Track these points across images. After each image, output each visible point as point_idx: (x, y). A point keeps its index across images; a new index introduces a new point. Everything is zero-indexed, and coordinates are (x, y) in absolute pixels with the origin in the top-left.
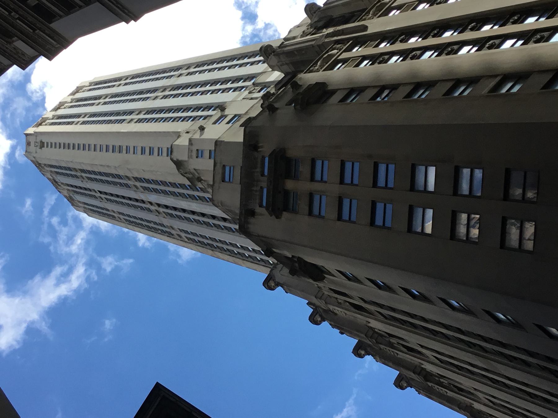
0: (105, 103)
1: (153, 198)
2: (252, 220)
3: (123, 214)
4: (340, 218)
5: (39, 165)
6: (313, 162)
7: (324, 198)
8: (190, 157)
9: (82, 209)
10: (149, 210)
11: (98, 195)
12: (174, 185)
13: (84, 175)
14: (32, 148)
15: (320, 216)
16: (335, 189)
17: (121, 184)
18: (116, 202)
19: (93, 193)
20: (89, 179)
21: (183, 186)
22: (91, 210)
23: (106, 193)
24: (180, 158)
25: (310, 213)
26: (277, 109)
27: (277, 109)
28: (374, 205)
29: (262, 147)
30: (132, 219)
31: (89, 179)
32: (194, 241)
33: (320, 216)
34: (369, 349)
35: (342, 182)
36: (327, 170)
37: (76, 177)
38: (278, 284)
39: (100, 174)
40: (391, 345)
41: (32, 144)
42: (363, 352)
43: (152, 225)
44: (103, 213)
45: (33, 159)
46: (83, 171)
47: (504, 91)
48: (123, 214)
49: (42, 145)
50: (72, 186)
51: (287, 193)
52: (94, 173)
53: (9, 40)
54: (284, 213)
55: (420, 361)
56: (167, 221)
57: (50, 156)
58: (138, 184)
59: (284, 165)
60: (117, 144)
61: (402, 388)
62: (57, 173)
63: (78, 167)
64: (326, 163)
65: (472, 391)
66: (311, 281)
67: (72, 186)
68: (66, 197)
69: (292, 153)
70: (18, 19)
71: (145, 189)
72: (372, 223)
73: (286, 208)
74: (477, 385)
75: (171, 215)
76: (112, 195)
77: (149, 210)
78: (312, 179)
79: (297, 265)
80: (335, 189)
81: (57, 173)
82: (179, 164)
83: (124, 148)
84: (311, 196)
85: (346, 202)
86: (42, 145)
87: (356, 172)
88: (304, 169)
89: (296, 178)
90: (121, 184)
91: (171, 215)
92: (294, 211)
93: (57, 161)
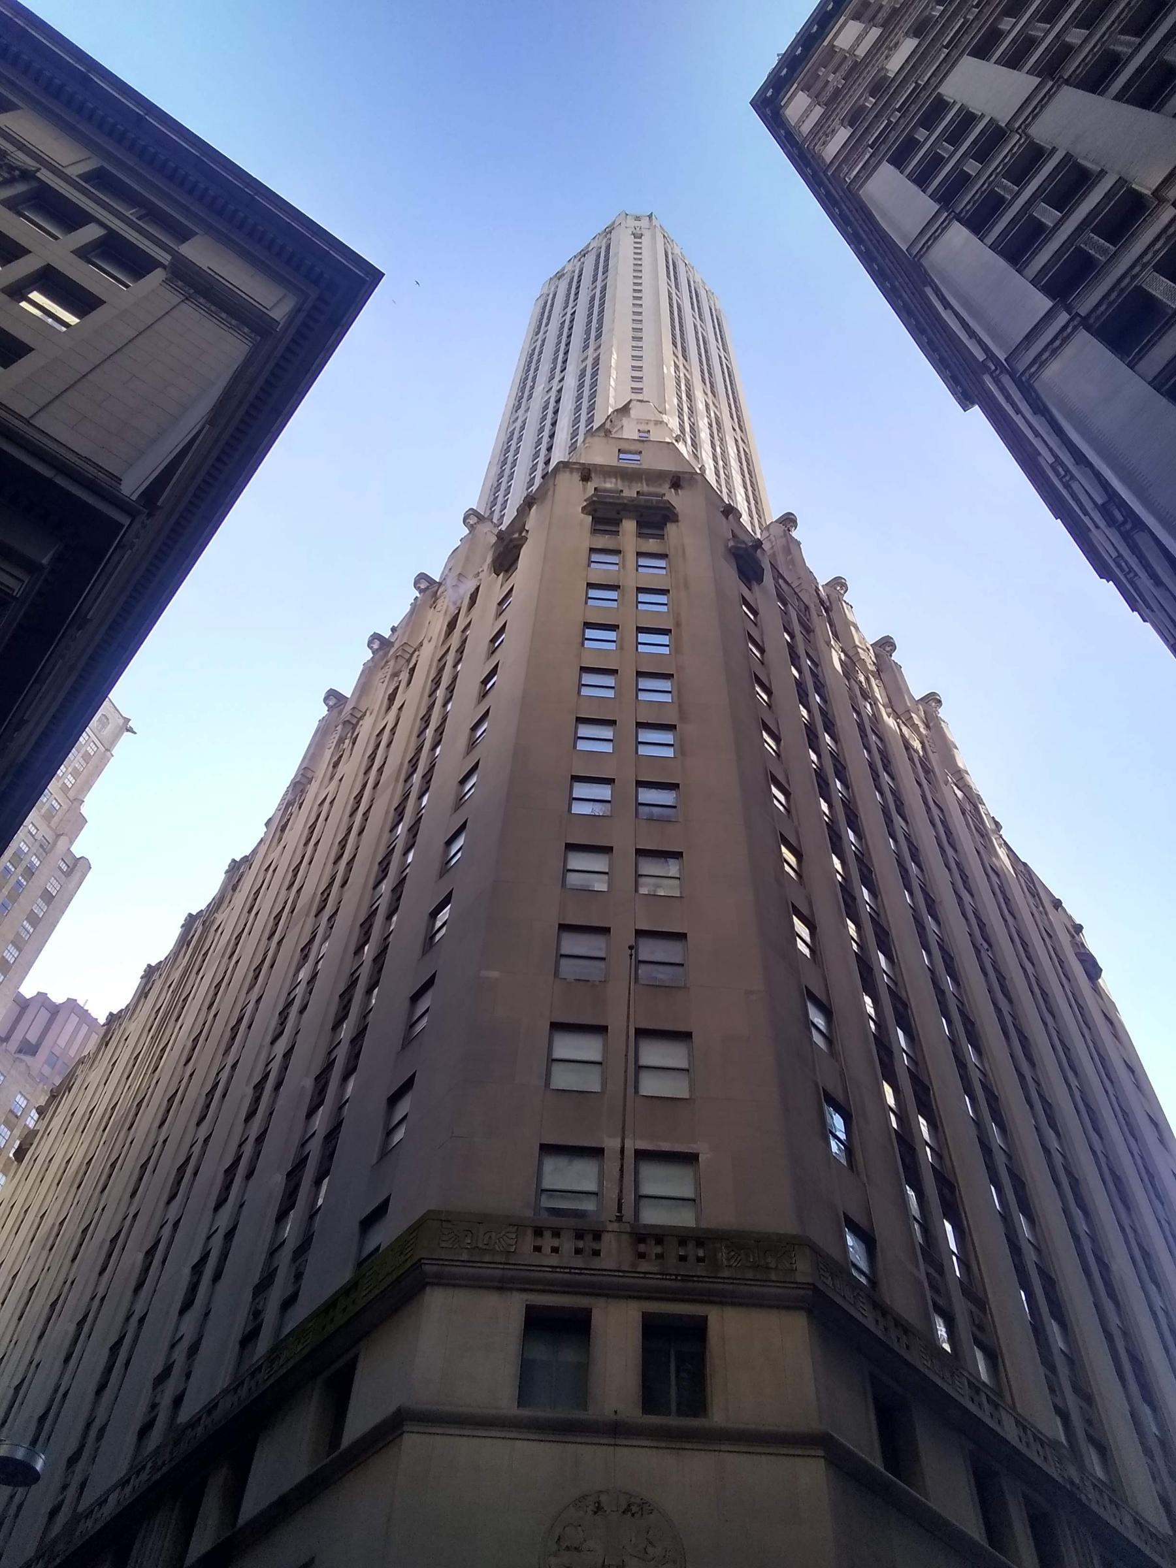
0: (695, 326)
1: (571, 382)
2: (576, 477)
3: (542, 345)
4: (590, 586)
5: (609, 231)
6: (663, 556)
7: (616, 568)
8: (639, 421)
9: (545, 291)
10: (552, 378)
11: (569, 311)
12: (592, 408)
13: (598, 291)
14: (631, 223)
15: (590, 562)
16: (630, 581)
17: (587, 339)
18: (561, 335)
19: (571, 304)
20: (593, 299)
21: (590, 420)
22: (546, 303)
23: (572, 321)
24: (632, 412)
25: (592, 550)
26: (727, 518)
27: (727, 518)
28: (613, 628)
29: (677, 493)
30: (535, 357)
31: (593, 299)
32: (510, 439)
33: (590, 562)
34: (381, 653)
35: (640, 590)
36: (654, 572)
37: (595, 280)
38: (472, 528)
39: (601, 311)
40: (341, 741)
41: (637, 223)
42: (376, 646)
43: (529, 383)
44: (542, 319)
45: (617, 223)
46: (604, 288)
47: (775, 791)
48: (542, 345)
49: (638, 236)
50: (580, 276)
51: (617, 522)
52: (602, 304)
53: (846, 123)
54: (590, 518)
55: (377, 709)
56: (536, 404)
57: (624, 247)
58: (590, 362)
59: (655, 519)
60: (644, 335)
61: (326, 700)
62: (598, 256)
63: (609, 281)
64: (663, 572)
65: (282, 843)
66: (489, 560)
67: (580, 276)
68: (563, 269)
69: (671, 529)
70: (918, 85)
71: (583, 371)
72: (588, 625)
73: (595, 520)
74: (237, 912)
75: (546, 407)
76: (571, 328)
77: (552, 378)
78: (640, 554)
79: (516, 535)
80: (630, 581)
81: (598, 256)
82: (625, 410)
83: (640, 344)
84: (617, 552)
85: (613, 595)
86: (638, 236)
87: (654, 608)
88: (652, 545)
89: (640, 535)
90: (587, 339)
91: (546, 407)
92: (594, 531)
93: (617, 254)
